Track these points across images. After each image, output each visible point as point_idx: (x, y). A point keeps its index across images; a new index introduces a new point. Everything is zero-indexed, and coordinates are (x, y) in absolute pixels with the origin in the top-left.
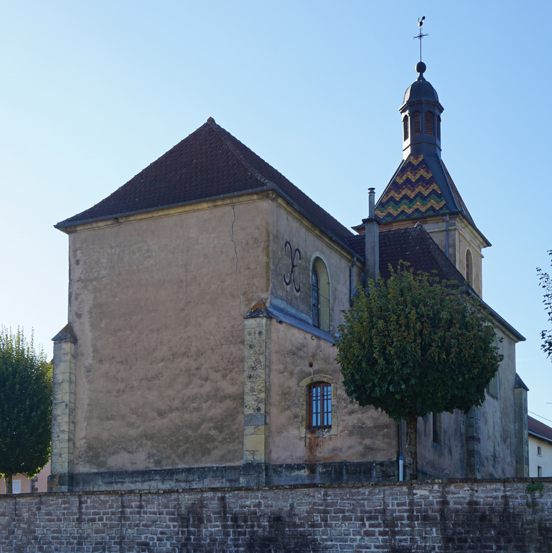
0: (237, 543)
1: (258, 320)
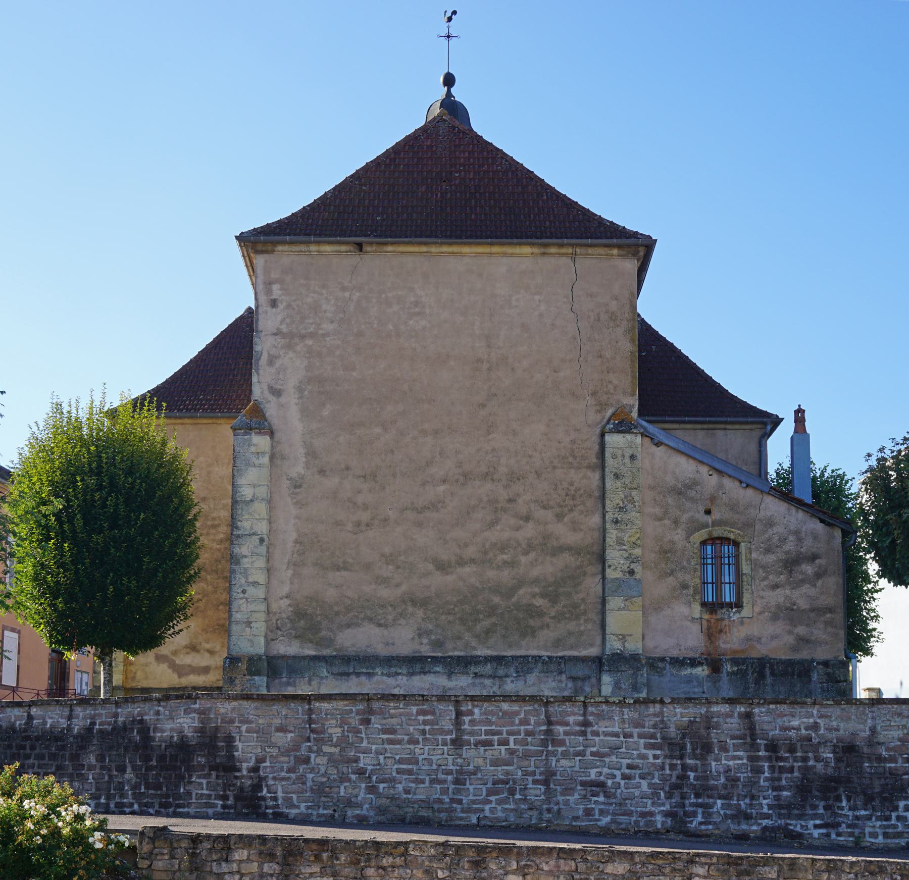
0: (776, 784)
1: (629, 437)
